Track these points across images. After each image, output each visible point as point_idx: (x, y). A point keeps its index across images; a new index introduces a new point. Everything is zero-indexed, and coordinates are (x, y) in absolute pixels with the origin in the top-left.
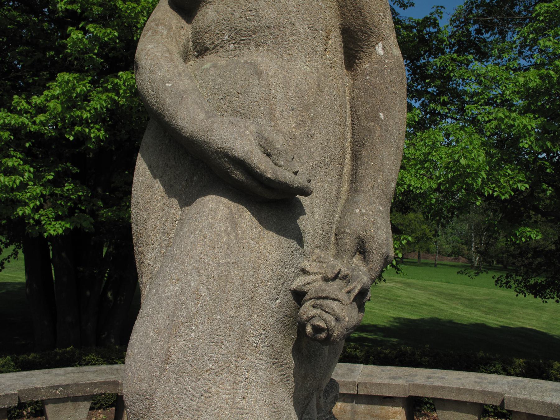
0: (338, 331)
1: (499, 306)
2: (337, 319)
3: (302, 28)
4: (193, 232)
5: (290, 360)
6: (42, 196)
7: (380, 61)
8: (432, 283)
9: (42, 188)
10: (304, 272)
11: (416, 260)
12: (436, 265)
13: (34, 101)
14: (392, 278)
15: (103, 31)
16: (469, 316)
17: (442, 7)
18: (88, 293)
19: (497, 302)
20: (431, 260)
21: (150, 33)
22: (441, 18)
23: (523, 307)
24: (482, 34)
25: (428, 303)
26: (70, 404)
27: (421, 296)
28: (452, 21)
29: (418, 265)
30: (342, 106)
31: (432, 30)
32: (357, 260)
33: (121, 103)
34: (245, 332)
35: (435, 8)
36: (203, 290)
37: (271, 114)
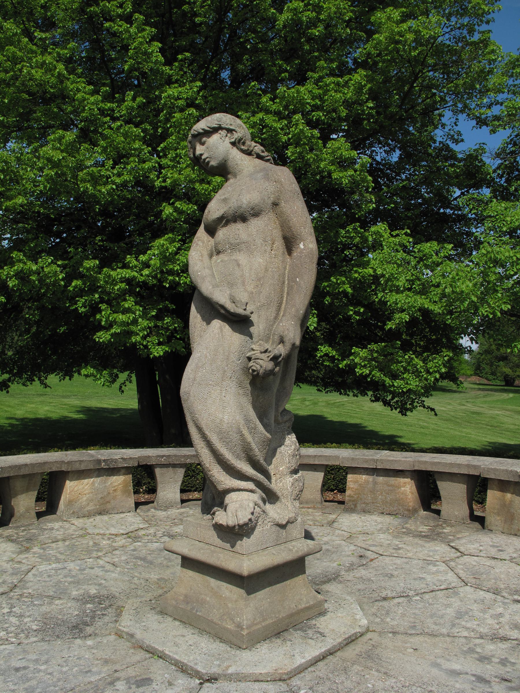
0: (261, 371)
2: (261, 367)
3: (259, 242)
6: (149, 328)
7: (301, 252)
9: (148, 322)
10: (253, 350)
13: (141, 259)
15: (187, 206)
17: (484, 144)
26: (171, 469)
34: (225, 371)
35: (478, 145)
36: (208, 354)
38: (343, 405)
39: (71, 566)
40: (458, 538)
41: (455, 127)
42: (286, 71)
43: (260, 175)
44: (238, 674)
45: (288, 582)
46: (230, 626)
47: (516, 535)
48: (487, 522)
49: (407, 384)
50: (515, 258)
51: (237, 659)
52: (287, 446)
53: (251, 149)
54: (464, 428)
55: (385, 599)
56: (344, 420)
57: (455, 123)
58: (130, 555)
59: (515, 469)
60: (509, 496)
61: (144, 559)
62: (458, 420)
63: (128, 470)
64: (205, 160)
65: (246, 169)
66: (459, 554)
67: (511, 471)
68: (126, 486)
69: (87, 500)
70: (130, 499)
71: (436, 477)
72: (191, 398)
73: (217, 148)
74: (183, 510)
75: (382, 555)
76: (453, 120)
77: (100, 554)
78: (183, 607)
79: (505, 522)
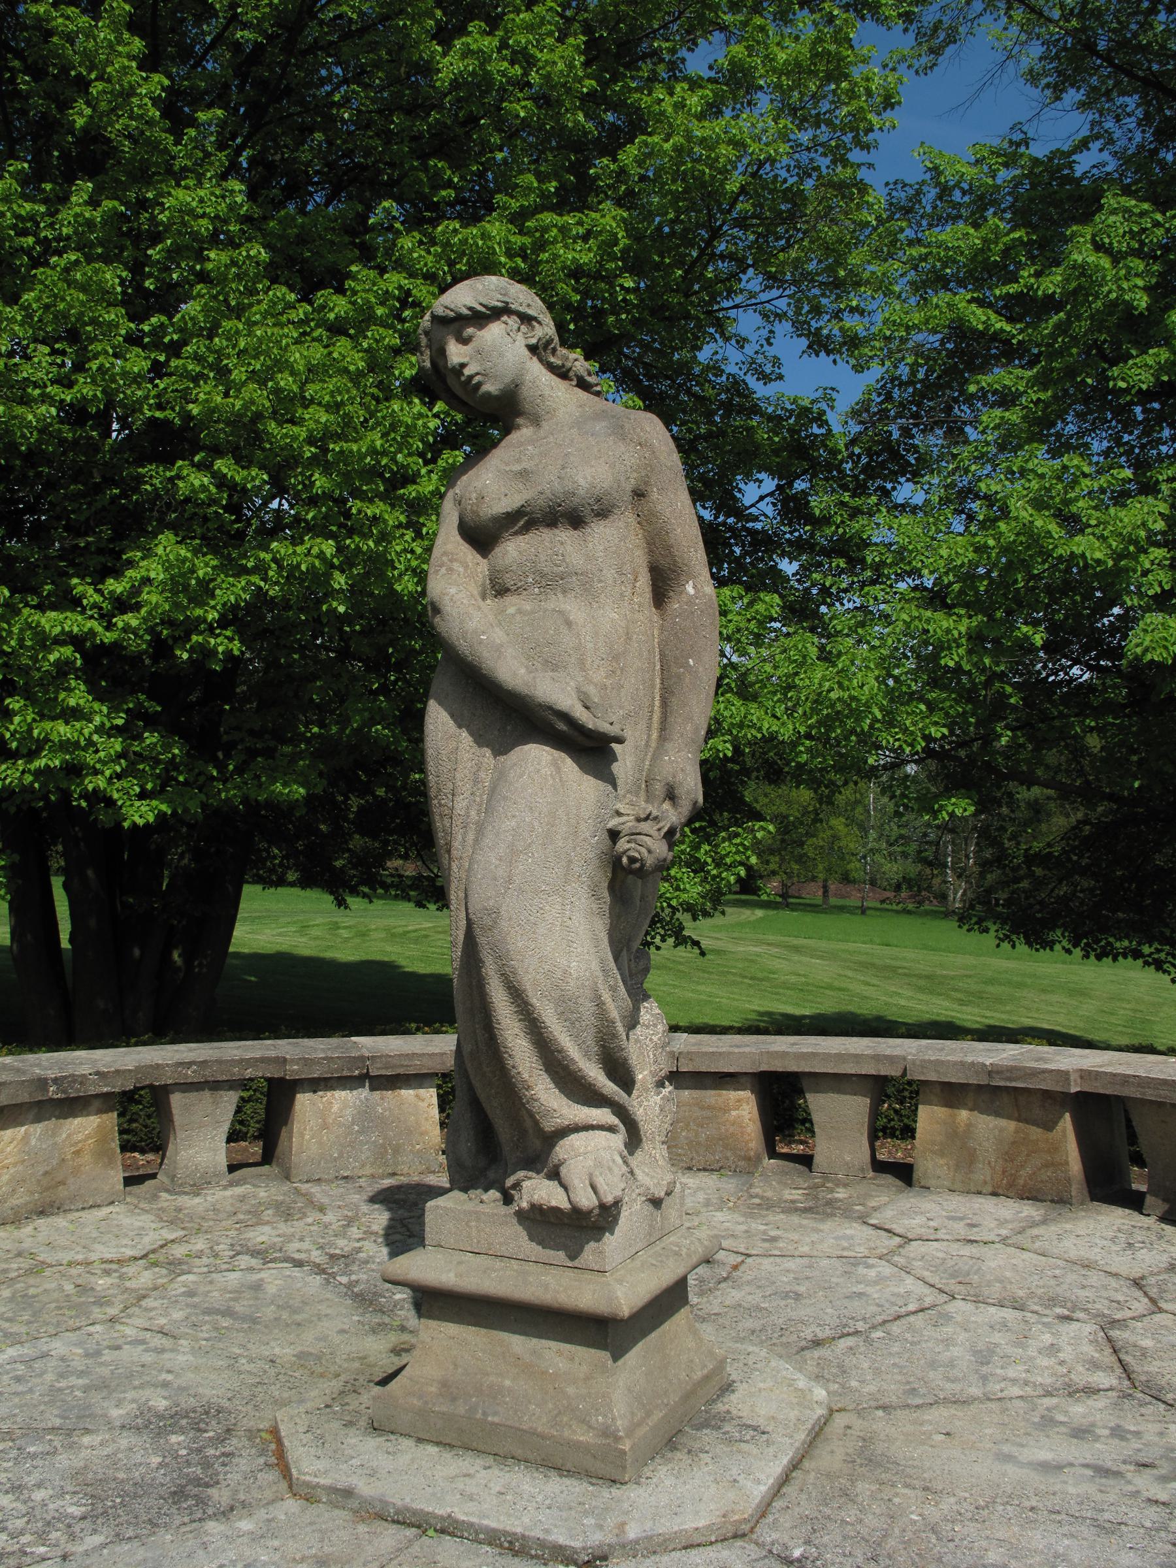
0: (650, 861)
1: (990, 989)
2: (649, 851)
3: (609, 574)
4: (521, 776)
5: (606, 894)
7: (690, 602)
8: (851, 946)
11: (819, 900)
12: (863, 911)
14: (761, 936)
15: (245, 473)
16: (924, 1008)
17: (833, 389)
18: (137, 952)
19: (991, 981)
20: (853, 902)
21: (443, 570)
22: (832, 408)
23: (1044, 991)
24: (913, 437)
25: (836, 984)
26: (207, 1094)
27: (821, 970)
28: (855, 414)
29: (824, 911)
30: (651, 652)
31: (816, 430)
32: (666, 806)
33: (271, 593)
35: (820, 391)
36: (536, 824)
37: (582, 664)
38: (426, 936)
39: (58, 1347)
40: (875, 1209)
41: (766, 347)
42: (449, 184)
43: (600, 426)
44: (649, 1538)
45: (666, 1326)
46: (584, 1436)
47: (979, 1193)
48: (917, 1174)
49: (678, 889)
50: (956, 633)
51: (626, 1505)
52: (647, 1027)
53: (568, 364)
54: (698, 983)
55: (817, 1343)
56: (441, 971)
57: (768, 340)
58: (187, 1305)
59: (980, 1060)
60: (964, 1114)
61: (228, 1313)
62: (681, 967)
63: (107, 1102)
64: (471, 377)
65: (563, 409)
66: (898, 1240)
67: (973, 1064)
68: (102, 1140)
69: (10, 1181)
70: (112, 1173)
71: (805, 1083)
72: (504, 924)
73: (501, 355)
74: (239, 1190)
75: (748, 1255)
76: (764, 333)
77: (112, 1311)
78: (444, 1409)
79: (957, 1167)
